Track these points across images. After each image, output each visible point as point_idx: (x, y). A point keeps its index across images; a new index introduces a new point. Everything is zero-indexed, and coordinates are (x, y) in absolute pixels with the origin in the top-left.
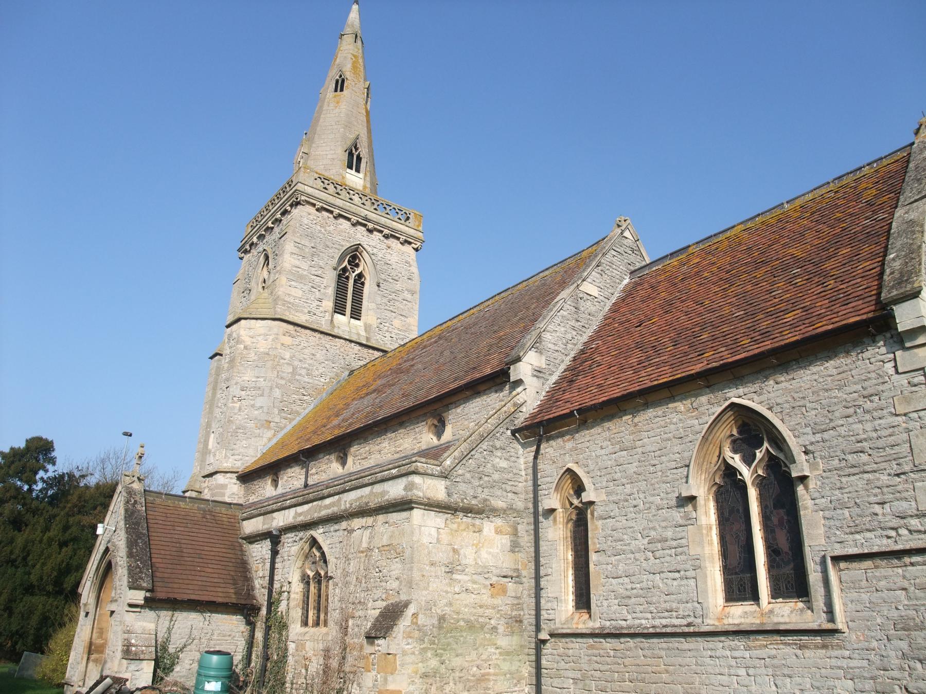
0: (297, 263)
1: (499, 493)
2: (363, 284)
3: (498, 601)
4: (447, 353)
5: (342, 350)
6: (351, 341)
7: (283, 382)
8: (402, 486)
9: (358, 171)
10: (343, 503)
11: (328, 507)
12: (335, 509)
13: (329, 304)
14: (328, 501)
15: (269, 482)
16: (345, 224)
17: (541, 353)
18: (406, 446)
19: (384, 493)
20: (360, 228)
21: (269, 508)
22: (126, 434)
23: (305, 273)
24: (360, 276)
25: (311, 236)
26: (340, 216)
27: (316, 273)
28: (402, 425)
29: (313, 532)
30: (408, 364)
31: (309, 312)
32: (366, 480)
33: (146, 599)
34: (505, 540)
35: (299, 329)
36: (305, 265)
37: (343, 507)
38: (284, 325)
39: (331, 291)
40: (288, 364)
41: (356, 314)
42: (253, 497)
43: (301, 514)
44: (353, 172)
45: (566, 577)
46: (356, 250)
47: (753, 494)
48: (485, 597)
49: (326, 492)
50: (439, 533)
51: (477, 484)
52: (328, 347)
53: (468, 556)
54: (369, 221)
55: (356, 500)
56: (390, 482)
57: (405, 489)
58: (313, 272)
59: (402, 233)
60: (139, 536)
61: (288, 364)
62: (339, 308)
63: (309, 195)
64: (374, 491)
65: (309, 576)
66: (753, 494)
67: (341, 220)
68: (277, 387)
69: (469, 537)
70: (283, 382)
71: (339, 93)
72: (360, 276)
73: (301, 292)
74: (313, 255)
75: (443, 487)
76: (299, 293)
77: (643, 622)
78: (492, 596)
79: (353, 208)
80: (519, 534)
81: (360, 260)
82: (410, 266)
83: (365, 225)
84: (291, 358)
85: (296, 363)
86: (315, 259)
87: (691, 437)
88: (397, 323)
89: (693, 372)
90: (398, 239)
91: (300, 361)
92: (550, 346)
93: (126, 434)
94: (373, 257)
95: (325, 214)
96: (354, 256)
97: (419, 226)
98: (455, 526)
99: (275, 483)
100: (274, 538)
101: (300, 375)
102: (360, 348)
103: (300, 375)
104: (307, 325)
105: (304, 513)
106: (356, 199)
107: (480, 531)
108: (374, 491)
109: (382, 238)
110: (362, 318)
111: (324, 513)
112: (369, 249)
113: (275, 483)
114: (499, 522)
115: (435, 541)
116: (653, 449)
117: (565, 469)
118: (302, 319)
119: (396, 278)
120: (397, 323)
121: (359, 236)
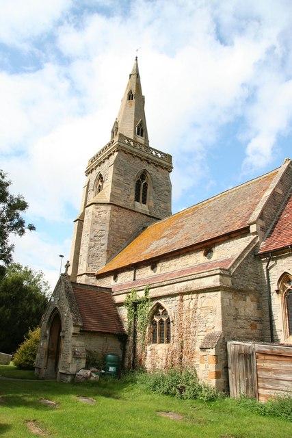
3: (254, 331)
4: (203, 219)
6: (143, 214)
9: (142, 136)
13: (133, 197)
15: (112, 277)
19: (201, 283)
22: (61, 256)
24: (146, 184)
25: (124, 166)
28: (184, 254)
29: (159, 301)
30: (180, 224)
32: (189, 278)
33: (80, 331)
36: (122, 179)
39: (133, 191)
41: (144, 202)
48: (249, 330)
53: (242, 312)
62: (137, 199)
63: (159, 163)
65: (156, 322)
67: (136, 158)
69: (241, 302)
71: (131, 101)
72: (146, 184)
76: (119, 192)
78: (252, 329)
88: (162, 205)
93: (61, 256)
96: (143, 175)
98: (235, 298)
99: (115, 278)
106: (143, 148)
107: (245, 300)
113: (115, 278)
114: (252, 296)
118: (121, 204)
120: (162, 205)
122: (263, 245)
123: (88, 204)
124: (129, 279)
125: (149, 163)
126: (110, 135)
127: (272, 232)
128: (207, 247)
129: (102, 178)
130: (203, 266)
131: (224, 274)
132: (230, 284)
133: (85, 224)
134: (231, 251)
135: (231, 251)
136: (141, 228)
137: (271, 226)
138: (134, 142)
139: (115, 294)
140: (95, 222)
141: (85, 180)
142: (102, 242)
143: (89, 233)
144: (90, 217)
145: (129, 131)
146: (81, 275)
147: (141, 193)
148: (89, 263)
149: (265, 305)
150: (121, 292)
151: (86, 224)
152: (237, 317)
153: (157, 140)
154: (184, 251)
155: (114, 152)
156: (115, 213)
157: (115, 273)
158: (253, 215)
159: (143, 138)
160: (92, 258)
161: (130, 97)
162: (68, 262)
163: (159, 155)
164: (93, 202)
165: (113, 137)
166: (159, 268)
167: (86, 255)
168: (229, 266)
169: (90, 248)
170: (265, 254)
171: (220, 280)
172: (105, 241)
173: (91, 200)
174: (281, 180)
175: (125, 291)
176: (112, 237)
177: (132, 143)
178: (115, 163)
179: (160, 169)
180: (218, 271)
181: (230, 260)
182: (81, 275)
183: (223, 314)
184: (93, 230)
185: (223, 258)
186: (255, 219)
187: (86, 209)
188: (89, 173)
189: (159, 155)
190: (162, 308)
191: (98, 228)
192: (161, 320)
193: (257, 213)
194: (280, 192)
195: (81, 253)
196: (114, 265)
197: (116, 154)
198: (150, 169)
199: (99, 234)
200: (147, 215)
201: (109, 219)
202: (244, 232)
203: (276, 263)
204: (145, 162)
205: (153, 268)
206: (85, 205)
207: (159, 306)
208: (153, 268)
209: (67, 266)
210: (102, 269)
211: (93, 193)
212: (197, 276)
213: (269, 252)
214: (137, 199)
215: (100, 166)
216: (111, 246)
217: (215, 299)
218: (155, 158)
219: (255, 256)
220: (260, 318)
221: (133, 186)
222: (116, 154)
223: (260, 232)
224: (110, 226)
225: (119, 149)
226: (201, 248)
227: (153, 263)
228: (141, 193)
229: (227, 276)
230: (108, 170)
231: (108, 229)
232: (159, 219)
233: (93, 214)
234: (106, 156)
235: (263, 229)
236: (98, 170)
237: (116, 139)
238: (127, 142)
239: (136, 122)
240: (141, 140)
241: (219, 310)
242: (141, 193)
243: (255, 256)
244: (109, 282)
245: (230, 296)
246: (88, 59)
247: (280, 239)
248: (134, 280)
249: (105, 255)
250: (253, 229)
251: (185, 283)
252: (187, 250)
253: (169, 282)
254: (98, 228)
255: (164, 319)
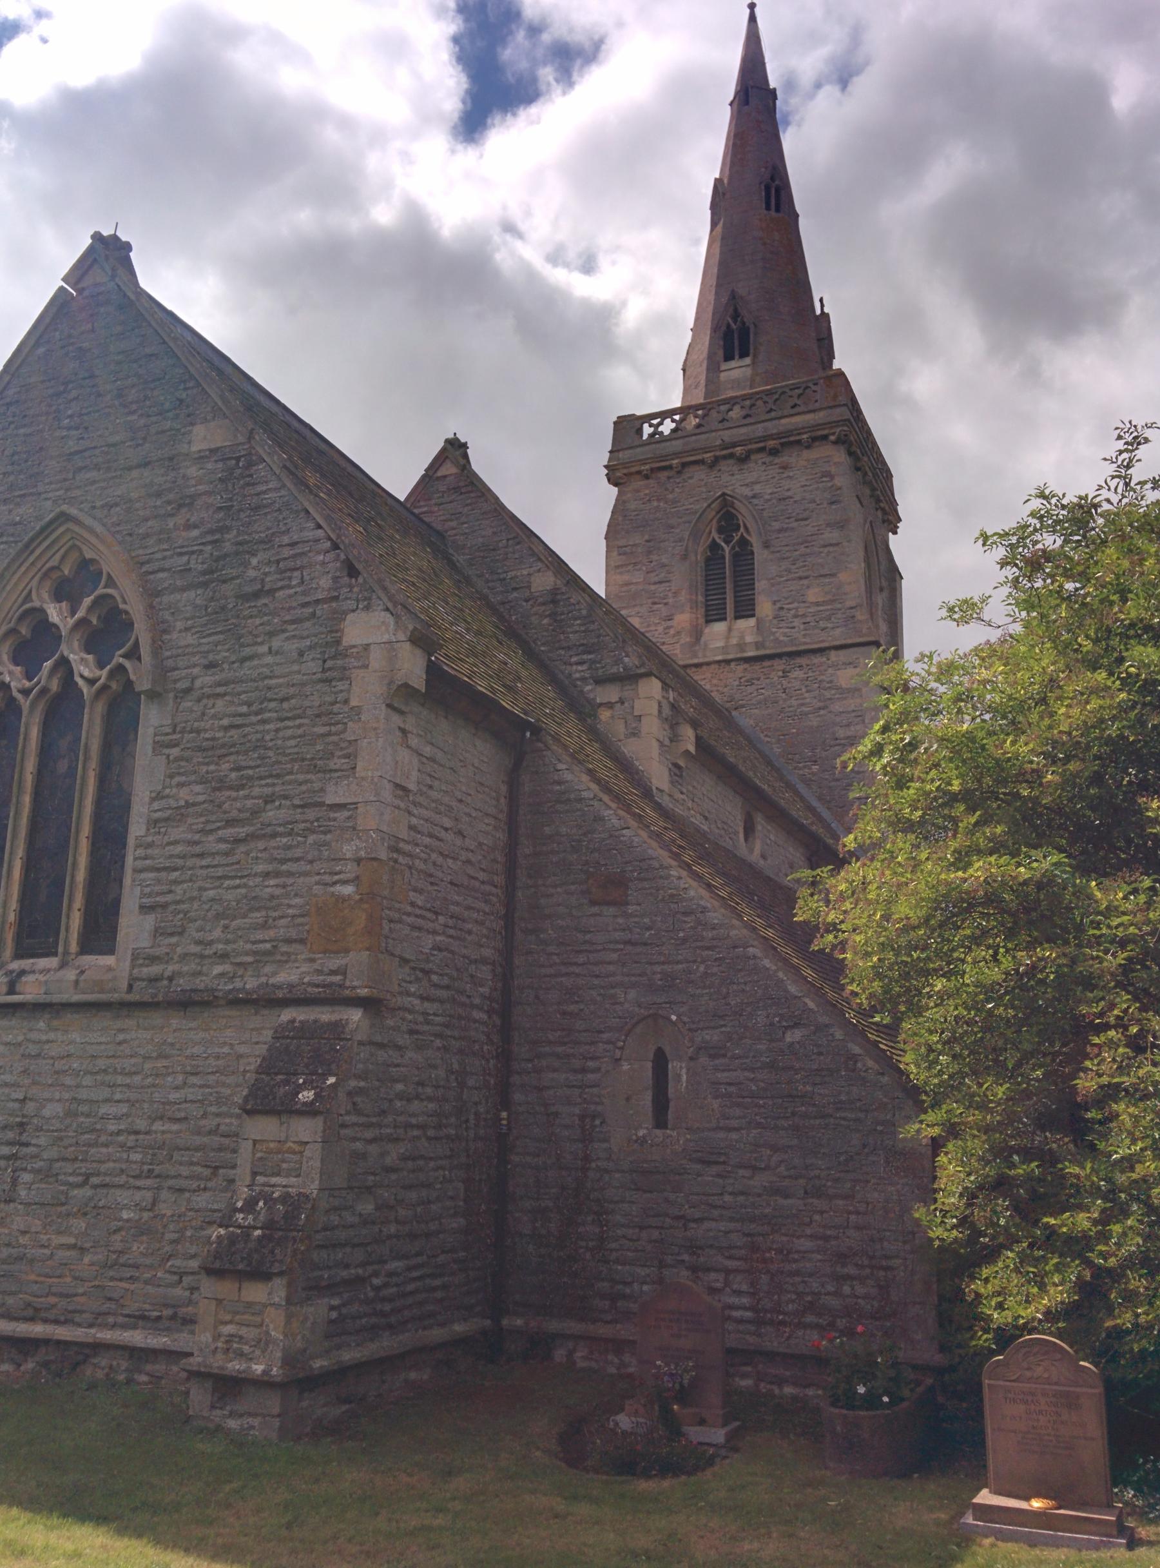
5: (715, 681)
16: (698, 475)
20: (724, 466)
26: (684, 465)
27: (656, 579)
36: (638, 577)
47: (736, 336)
54: (734, 445)
59: (800, 431)
66: (736, 336)
74: (649, 553)
77: (729, 809)
82: (832, 477)
83: (731, 456)
95: (663, 475)
97: (835, 397)
102: (746, 666)
119: (805, 515)
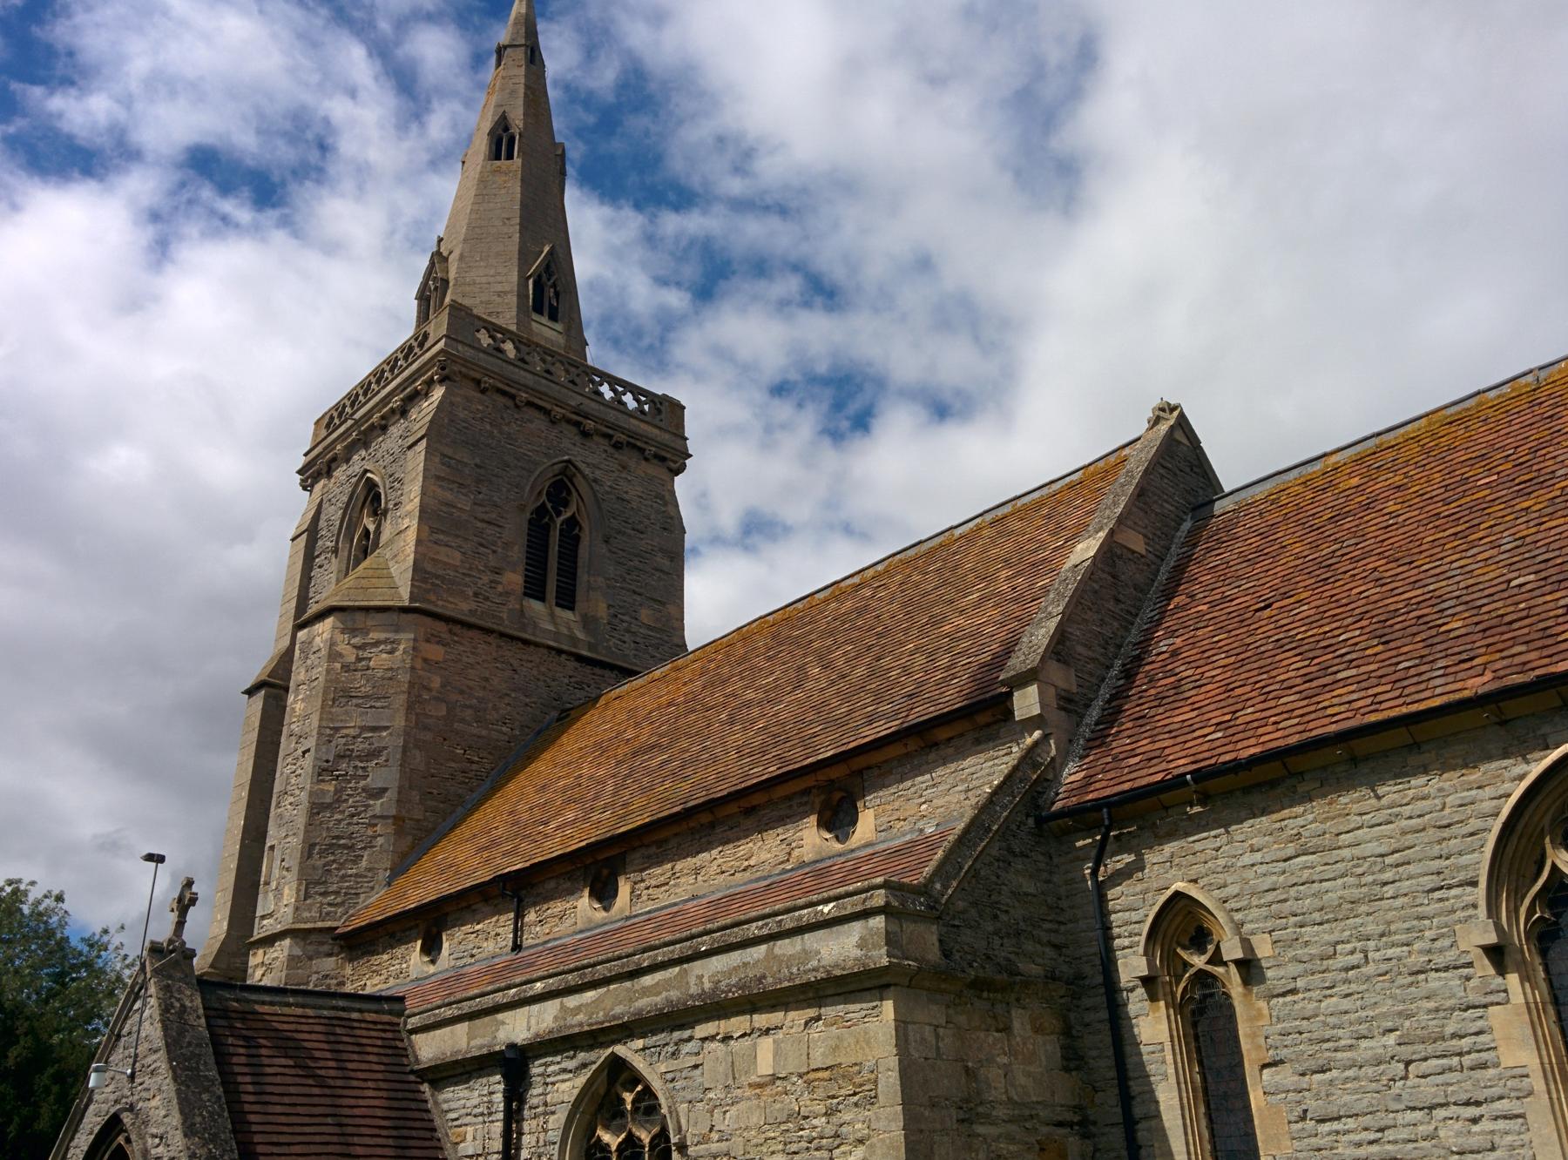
0: (449, 496)
1: (1029, 946)
2: (577, 539)
6: (560, 652)
7: (428, 736)
8: (855, 939)
9: (553, 317)
10: (693, 980)
11: (655, 991)
12: (674, 994)
13: (514, 579)
14: (647, 980)
17: (1066, 663)
18: (764, 856)
21: (488, 1001)
22: (150, 857)
23: (464, 517)
24: (572, 522)
27: (486, 517)
29: (620, 1050)
31: (476, 595)
32: (754, 930)
34: (1048, 1048)
35: (457, 629)
36: (464, 503)
37: (694, 990)
38: (428, 620)
39: (518, 553)
40: (436, 699)
41: (567, 599)
42: (376, 980)
43: (578, 1009)
44: (545, 320)
45: (1259, 1109)
46: (563, 472)
49: (646, 960)
50: (937, 1036)
51: (991, 929)
52: (516, 663)
55: (729, 973)
56: (821, 933)
57: (860, 946)
58: (480, 516)
60: (595, 1038)
61: (436, 699)
62: (535, 589)
64: (777, 951)
67: (531, 413)
68: (416, 747)
70: (428, 736)
71: (503, 163)
72: (572, 522)
73: (458, 555)
75: (935, 939)
76: (456, 558)
79: (554, 390)
80: (1074, 1032)
81: (569, 493)
84: (443, 686)
85: (454, 697)
86: (484, 490)
87: (1475, 824)
89: (1466, 694)
90: (642, 451)
91: (462, 692)
92: (1080, 649)
93: (150, 857)
94: (597, 488)
95: (501, 400)
96: (561, 488)
98: (962, 1019)
99: (431, 948)
100: (514, 1066)
101: (463, 720)
102: (577, 665)
103: (463, 720)
104: (472, 620)
105: (586, 1009)
107: (1006, 1029)
108: (777, 951)
109: (611, 450)
110: (578, 605)
111: (644, 1003)
112: (587, 471)
113: (431, 948)
115: (932, 1054)
116: (1382, 850)
117: (1169, 893)
118: (462, 607)
119: (640, 527)
120: (645, 615)
121: (566, 443)
122: (1072, 774)
123: (313, 609)
124: (490, 946)
125: (585, 434)
126: (411, 308)
127: (1112, 715)
128: (831, 790)
129: (377, 497)
130: (818, 870)
131: (905, 905)
132: (934, 954)
133: (297, 703)
134: (928, 809)
135: (928, 809)
136: (555, 714)
137: (1105, 692)
138: (518, 341)
139: (413, 1022)
140: (337, 695)
141: (300, 504)
142: (375, 779)
143: (311, 743)
144: (320, 671)
145: (496, 290)
146: (269, 941)
147: (554, 549)
148: (311, 884)
149: (1097, 1043)
150: (448, 1013)
151: (300, 705)
152: (970, 1111)
153: (425, 157)
154: (733, 808)
155: (430, 383)
156: (436, 652)
157: (427, 925)
158: (1024, 645)
159: (558, 326)
160: (323, 861)
161: (501, 142)
162: (189, 883)
163: (628, 399)
164: (334, 602)
165: (423, 317)
166: (624, 888)
167: (295, 842)
168: (927, 871)
169: (317, 808)
170: (1086, 816)
171: (891, 940)
172: (383, 775)
173: (327, 590)
174: (1141, 493)
175: (466, 1007)
176: (418, 758)
177: (509, 347)
178: (436, 432)
179: (632, 460)
180: (879, 897)
181: (930, 844)
182: (269, 941)
183: (907, 1102)
184: (328, 732)
185: (903, 835)
186: (1033, 660)
187: (301, 635)
188: (316, 477)
189: (628, 399)
190: (635, 1078)
191: (354, 720)
192: (631, 1141)
193: (1041, 635)
194: (1137, 543)
195: (274, 835)
196: (423, 887)
197: (438, 393)
198: (591, 459)
199: (360, 746)
200: (580, 658)
201: (404, 678)
202: (983, 716)
203: (1139, 865)
204: (570, 431)
205: (604, 894)
206: (297, 617)
207: (618, 1071)
208: (604, 894)
209: (185, 903)
210: (376, 903)
211: (335, 565)
212: (788, 921)
213: (1098, 805)
214: (535, 589)
215: (366, 446)
216: (415, 796)
217: (872, 1033)
218: (612, 416)
219: (1031, 824)
220: (1078, 1108)
221: (515, 531)
222: (438, 393)
223: (1057, 717)
224: (410, 708)
225: (448, 370)
226: (807, 792)
227: (597, 867)
228: (554, 549)
229: (917, 917)
230: (405, 467)
231: (399, 722)
232: (630, 673)
233: (333, 655)
234: (396, 402)
235: (1069, 704)
236: (358, 463)
237: (439, 326)
238: (485, 340)
239: (525, 257)
240: (546, 331)
241: (890, 1081)
242: (552, 560)
243: (1040, 821)
244: (405, 969)
245: (937, 1013)
246: (1057, 654)
247: (1144, 745)
248: (517, 947)
249: (384, 838)
250: (1027, 702)
251: (735, 957)
252: (745, 803)
253: (661, 955)
254: (354, 720)
255: (645, 1137)
